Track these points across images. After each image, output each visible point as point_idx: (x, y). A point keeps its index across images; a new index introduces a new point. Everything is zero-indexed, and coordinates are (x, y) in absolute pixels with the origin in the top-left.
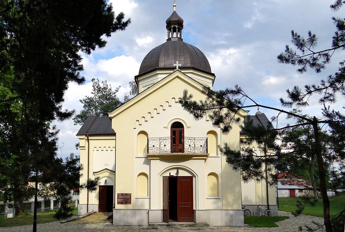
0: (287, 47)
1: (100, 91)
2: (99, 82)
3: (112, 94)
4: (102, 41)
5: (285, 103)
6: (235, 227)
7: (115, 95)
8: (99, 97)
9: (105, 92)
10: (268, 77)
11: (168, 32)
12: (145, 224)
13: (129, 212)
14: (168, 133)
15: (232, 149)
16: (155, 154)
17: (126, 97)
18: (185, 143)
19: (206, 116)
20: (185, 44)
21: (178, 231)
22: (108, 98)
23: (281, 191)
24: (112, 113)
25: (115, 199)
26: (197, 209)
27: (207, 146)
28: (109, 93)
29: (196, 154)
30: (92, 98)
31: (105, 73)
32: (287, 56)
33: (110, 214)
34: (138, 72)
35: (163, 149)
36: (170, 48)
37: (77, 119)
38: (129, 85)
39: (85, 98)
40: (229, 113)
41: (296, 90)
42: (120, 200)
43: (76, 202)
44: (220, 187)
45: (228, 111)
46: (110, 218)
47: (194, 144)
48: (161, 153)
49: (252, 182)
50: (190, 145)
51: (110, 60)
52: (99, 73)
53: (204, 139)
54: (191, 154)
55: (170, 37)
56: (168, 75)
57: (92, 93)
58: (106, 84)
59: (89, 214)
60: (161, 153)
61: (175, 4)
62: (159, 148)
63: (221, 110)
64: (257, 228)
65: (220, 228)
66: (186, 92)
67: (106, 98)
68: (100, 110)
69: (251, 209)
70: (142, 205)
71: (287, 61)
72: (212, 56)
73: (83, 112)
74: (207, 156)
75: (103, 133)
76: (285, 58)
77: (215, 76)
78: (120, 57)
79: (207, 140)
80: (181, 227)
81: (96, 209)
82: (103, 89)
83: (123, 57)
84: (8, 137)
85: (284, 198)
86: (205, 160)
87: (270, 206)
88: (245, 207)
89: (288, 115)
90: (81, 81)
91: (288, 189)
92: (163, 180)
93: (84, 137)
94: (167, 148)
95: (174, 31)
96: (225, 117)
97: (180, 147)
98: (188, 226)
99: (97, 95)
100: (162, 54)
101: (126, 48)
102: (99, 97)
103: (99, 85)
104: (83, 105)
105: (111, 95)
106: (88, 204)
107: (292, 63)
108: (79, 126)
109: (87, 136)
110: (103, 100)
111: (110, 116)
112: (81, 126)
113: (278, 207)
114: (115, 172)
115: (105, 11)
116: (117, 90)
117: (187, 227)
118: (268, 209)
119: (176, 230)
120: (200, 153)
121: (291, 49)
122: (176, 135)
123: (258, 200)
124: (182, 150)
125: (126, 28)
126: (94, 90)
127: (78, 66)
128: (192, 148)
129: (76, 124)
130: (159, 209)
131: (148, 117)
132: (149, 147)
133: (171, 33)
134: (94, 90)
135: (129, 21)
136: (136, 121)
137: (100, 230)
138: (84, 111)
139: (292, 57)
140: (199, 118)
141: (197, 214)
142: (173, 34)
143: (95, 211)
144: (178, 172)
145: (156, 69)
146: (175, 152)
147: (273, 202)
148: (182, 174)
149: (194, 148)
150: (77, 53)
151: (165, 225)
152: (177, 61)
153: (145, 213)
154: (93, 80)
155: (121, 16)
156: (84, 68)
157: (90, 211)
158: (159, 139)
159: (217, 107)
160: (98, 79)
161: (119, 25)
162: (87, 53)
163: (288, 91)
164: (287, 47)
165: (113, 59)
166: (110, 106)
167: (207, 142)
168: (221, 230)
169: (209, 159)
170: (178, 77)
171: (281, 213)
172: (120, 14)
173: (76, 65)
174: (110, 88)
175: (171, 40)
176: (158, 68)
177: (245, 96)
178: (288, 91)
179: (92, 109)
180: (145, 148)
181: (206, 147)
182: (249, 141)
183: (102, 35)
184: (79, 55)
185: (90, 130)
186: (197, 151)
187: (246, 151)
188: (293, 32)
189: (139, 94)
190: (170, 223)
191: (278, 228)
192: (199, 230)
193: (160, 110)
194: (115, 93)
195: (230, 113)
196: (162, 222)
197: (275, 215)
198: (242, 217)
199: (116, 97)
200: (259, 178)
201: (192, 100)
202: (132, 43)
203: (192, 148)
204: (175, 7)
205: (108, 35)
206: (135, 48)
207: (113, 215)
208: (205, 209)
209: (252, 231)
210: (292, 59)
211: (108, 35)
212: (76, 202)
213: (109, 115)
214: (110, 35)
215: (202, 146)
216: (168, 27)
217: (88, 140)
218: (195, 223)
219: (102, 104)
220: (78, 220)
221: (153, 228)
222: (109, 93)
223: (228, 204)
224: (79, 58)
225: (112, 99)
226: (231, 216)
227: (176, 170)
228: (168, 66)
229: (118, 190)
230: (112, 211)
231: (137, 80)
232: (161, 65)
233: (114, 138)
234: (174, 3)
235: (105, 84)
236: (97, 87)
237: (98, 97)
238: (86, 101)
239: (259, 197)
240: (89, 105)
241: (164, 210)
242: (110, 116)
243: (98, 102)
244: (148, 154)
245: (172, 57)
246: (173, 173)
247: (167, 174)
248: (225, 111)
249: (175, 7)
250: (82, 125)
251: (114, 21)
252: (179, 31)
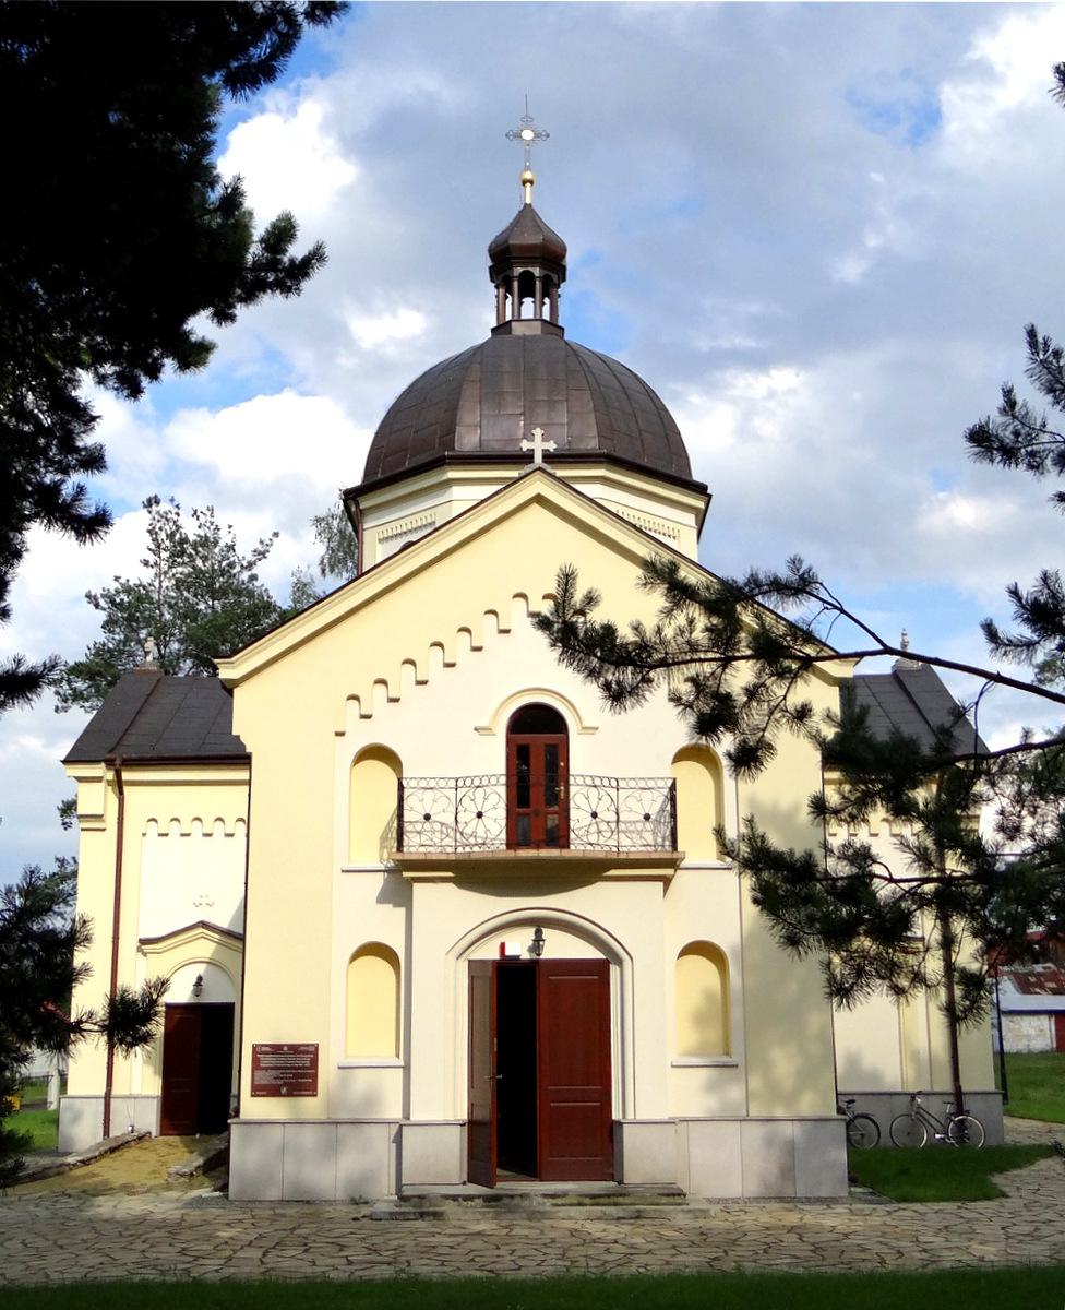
0: (1008, 393)
1: (182, 553)
2: (178, 514)
3: (238, 568)
4: (193, 338)
5: (1007, 645)
6: (809, 1201)
7: (254, 571)
8: (177, 580)
9: (205, 559)
10: (941, 495)
11: (497, 296)
12: (384, 1192)
13: (309, 1137)
14: (493, 757)
15: (777, 842)
16: (434, 853)
17: (301, 588)
18: (572, 804)
19: (664, 686)
20: (574, 352)
21: (538, 1224)
22: (218, 585)
23: (1019, 1024)
24: (233, 659)
25: (240, 1071)
26: (630, 1116)
27: (673, 816)
28: (224, 564)
29: (622, 856)
30: (144, 588)
31: (205, 474)
32: (1008, 433)
33: (216, 1143)
34: (362, 474)
35: (468, 830)
36: (507, 366)
37: (69, 682)
38: (314, 530)
39: (113, 586)
40: (763, 685)
41: (1049, 588)
42: (265, 1078)
43: (54, 1084)
44: (736, 1013)
45: (759, 676)
46: (217, 1165)
47: (613, 808)
48: (460, 850)
49: (876, 1002)
50: (594, 815)
51: (228, 414)
52: (176, 470)
53: (661, 783)
54: (602, 856)
55: (508, 318)
56: (502, 487)
57: (146, 563)
58: (212, 524)
59: (114, 1144)
60: (460, 850)
61: (528, 175)
62: (453, 825)
63: (723, 670)
64: (910, 1205)
65: (736, 1207)
66: (567, 576)
67: (210, 585)
68: (180, 641)
69: (879, 1112)
70: (371, 1100)
71: (1009, 454)
72: (695, 399)
73: (100, 651)
74: (673, 864)
75: (189, 753)
76: (1001, 442)
77: (710, 496)
78: (277, 396)
79: (673, 788)
80: (557, 1205)
81: (148, 1118)
82: (195, 546)
83: (288, 397)
85: (1031, 1055)
86: (667, 881)
87: (966, 1099)
89: (1039, 673)
90: (90, 525)
91: (1049, 1013)
92: (472, 979)
93: (98, 770)
94: (489, 829)
95: (527, 290)
96: (746, 703)
97: (552, 821)
98: (587, 1201)
99: (166, 573)
100: (471, 392)
101: (303, 358)
102: (177, 580)
103: (178, 528)
104: (102, 616)
105: (234, 571)
106: (108, 1097)
107: (1031, 467)
108: (80, 718)
109: (114, 765)
110: (195, 596)
112: (90, 717)
113: (1005, 1098)
114: (241, 938)
115: (209, 212)
116: (260, 548)
117: (580, 1204)
118: (960, 1110)
119: (528, 1223)
120: (643, 848)
121: (1025, 405)
122: (533, 761)
123: (910, 1072)
124: (560, 837)
125: (305, 285)
126: (153, 547)
127: (78, 450)
128: (603, 826)
129: (65, 710)
130: (450, 1118)
131: (402, 681)
132: (405, 819)
133: (509, 301)
134: (153, 547)
135: (316, 256)
136: (216, 820)
137: (163, 1225)
138: (104, 645)
139: (1031, 440)
140: (628, 704)
141: (630, 1137)
142: (521, 303)
143: (142, 1128)
144: (538, 939)
145: (444, 458)
146: (527, 844)
147: (979, 1076)
148: (560, 947)
149: (613, 826)
150: (74, 394)
151: (479, 1197)
152: (538, 429)
153: (381, 1140)
154: (152, 502)
155: (283, 232)
156: (106, 458)
157: (117, 1131)
158: (452, 783)
159: (711, 655)
160: (172, 500)
161: (275, 270)
162: (126, 392)
163: (1014, 593)
164: (1008, 393)
165: (245, 406)
166: (224, 627)
167: (673, 799)
168: (745, 1218)
169: (681, 879)
170: (539, 499)
171: (1021, 1129)
172: (280, 220)
173: (68, 445)
174: (230, 543)
175: (510, 333)
176: (451, 453)
177: (836, 607)
178: (1014, 593)
179: (142, 636)
180: (389, 826)
181: (668, 819)
182: (855, 811)
183: (194, 312)
184: (83, 401)
185: (131, 740)
186: (628, 842)
187: (843, 857)
188: (1032, 333)
189: (363, 575)
190: (503, 1187)
191: (1003, 1206)
192: (640, 1222)
193: (458, 647)
194: (251, 565)
195: (768, 683)
196: (464, 1183)
197: (993, 1142)
198: (841, 1156)
199: (257, 583)
200: (904, 983)
201: (597, 617)
202: (331, 335)
203: (603, 826)
204: (528, 185)
205: (224, 316)
206: (346, 361)
207: (227, 1150)
208: (664, 1117)
209: (888, 1220)
210: (1029, 449)
211: (224, 316)
212: (54, 1084)
214: (232, 318)
215: (653, 817)
216: (498, 274)
217: (119, 785)
218: (619, 1184)
219: (190, 613)
220: (59, 1174)
221: (422, 1215)
222: (224, 564)
223: (774, 1092)
224: (85, 417)
225: (239, 592)
226: (791, 1148)
227: (528, 934)
228: (495, 447)
229: (258, 1028)
230: (227, 1128)
231: (353, 509)
232: (465, 441)
233: (242, 775)
234: (527, 169)
235: (208, 524)
236: (171, 536)
237: (173, 581)
238: (118, 600)
239: (915, 1056)
240: (130, 619)
241: (473, 1125)
242: (226, 673)
243: (171, 606)
244: (399, 856)
245: (514, 407)
246: (518, 945)
247: (489, 952)
248: (741, 675)
249: (528, 185)
250: (95, 712)
251: (251, 250)
252: (545, 293)
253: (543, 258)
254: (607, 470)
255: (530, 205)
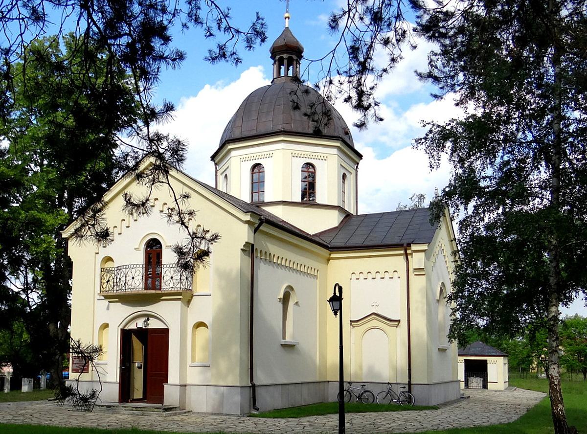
14: (139, 258)
61: (287, 15)
84: (7, 269)
88: (364, 385)
98: (134, 409)
111: (64, 236)
117: (132, 410)
118: (410, 391)
148: (154, 324)
204: (287, 19)
213: (63, 235)
234: (287, 12)
242: (64, 236)
249: (287, 19)
253: (286, 50)
254: (284, 137)
255: (288, 27)
